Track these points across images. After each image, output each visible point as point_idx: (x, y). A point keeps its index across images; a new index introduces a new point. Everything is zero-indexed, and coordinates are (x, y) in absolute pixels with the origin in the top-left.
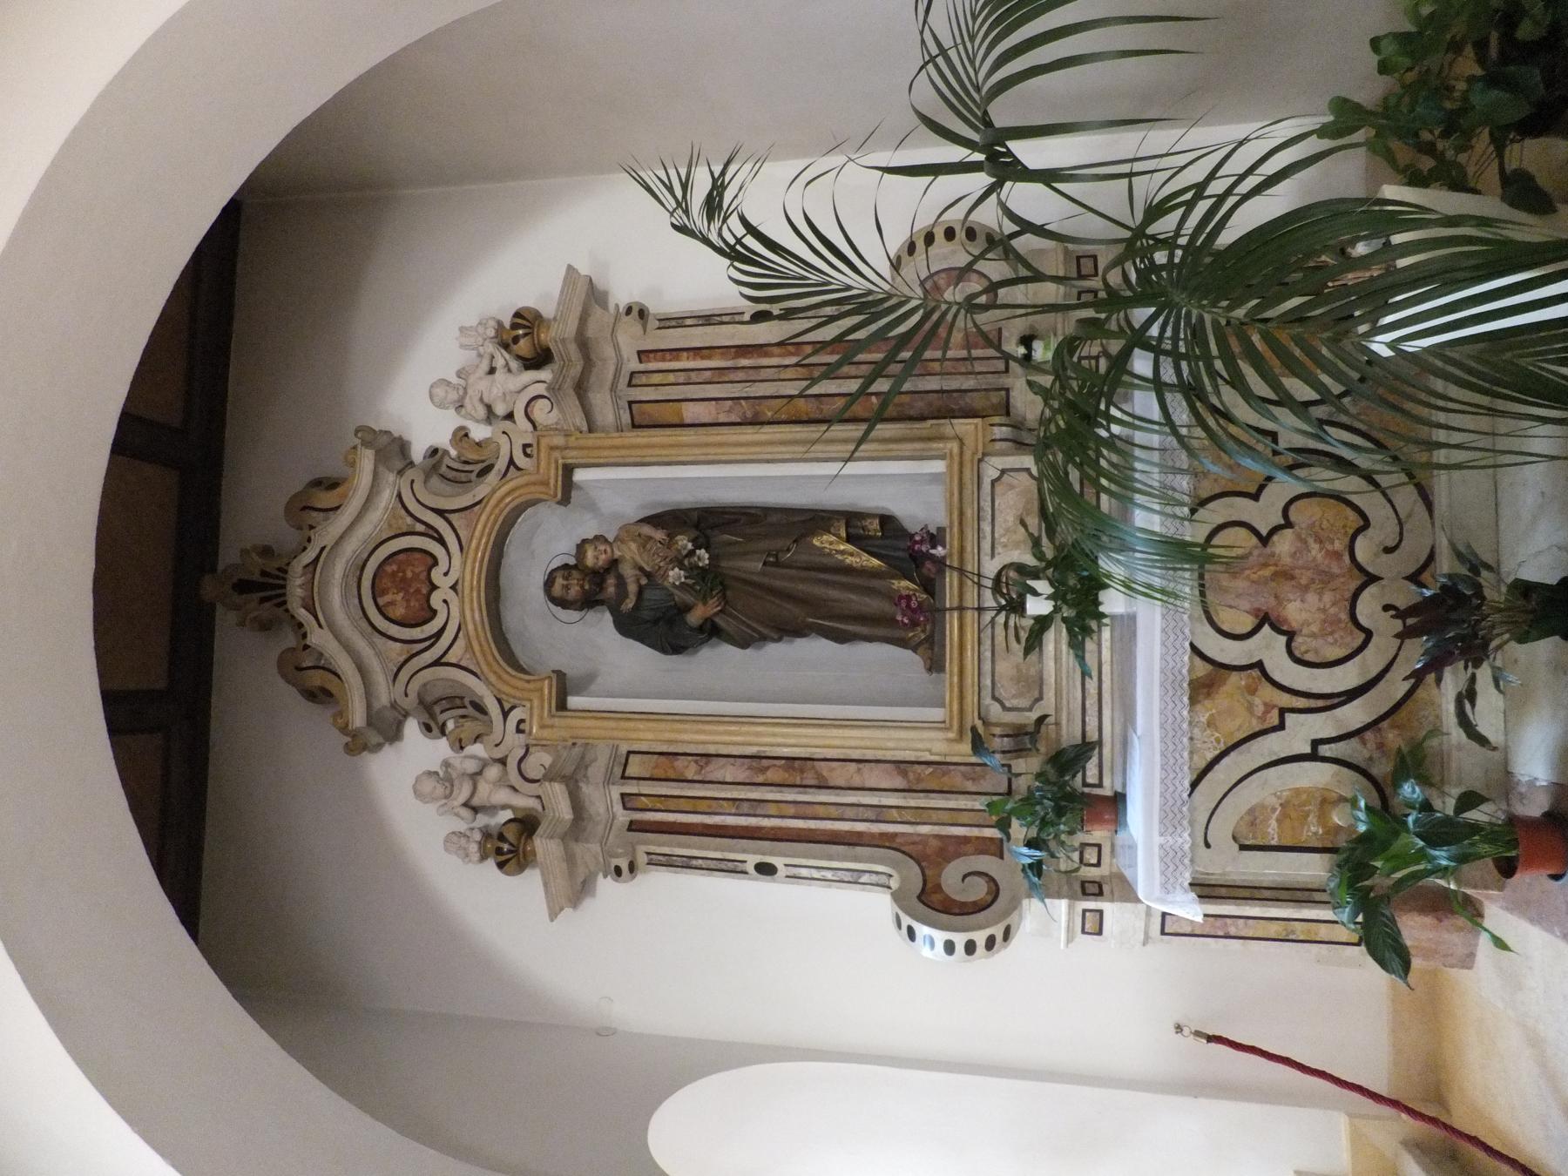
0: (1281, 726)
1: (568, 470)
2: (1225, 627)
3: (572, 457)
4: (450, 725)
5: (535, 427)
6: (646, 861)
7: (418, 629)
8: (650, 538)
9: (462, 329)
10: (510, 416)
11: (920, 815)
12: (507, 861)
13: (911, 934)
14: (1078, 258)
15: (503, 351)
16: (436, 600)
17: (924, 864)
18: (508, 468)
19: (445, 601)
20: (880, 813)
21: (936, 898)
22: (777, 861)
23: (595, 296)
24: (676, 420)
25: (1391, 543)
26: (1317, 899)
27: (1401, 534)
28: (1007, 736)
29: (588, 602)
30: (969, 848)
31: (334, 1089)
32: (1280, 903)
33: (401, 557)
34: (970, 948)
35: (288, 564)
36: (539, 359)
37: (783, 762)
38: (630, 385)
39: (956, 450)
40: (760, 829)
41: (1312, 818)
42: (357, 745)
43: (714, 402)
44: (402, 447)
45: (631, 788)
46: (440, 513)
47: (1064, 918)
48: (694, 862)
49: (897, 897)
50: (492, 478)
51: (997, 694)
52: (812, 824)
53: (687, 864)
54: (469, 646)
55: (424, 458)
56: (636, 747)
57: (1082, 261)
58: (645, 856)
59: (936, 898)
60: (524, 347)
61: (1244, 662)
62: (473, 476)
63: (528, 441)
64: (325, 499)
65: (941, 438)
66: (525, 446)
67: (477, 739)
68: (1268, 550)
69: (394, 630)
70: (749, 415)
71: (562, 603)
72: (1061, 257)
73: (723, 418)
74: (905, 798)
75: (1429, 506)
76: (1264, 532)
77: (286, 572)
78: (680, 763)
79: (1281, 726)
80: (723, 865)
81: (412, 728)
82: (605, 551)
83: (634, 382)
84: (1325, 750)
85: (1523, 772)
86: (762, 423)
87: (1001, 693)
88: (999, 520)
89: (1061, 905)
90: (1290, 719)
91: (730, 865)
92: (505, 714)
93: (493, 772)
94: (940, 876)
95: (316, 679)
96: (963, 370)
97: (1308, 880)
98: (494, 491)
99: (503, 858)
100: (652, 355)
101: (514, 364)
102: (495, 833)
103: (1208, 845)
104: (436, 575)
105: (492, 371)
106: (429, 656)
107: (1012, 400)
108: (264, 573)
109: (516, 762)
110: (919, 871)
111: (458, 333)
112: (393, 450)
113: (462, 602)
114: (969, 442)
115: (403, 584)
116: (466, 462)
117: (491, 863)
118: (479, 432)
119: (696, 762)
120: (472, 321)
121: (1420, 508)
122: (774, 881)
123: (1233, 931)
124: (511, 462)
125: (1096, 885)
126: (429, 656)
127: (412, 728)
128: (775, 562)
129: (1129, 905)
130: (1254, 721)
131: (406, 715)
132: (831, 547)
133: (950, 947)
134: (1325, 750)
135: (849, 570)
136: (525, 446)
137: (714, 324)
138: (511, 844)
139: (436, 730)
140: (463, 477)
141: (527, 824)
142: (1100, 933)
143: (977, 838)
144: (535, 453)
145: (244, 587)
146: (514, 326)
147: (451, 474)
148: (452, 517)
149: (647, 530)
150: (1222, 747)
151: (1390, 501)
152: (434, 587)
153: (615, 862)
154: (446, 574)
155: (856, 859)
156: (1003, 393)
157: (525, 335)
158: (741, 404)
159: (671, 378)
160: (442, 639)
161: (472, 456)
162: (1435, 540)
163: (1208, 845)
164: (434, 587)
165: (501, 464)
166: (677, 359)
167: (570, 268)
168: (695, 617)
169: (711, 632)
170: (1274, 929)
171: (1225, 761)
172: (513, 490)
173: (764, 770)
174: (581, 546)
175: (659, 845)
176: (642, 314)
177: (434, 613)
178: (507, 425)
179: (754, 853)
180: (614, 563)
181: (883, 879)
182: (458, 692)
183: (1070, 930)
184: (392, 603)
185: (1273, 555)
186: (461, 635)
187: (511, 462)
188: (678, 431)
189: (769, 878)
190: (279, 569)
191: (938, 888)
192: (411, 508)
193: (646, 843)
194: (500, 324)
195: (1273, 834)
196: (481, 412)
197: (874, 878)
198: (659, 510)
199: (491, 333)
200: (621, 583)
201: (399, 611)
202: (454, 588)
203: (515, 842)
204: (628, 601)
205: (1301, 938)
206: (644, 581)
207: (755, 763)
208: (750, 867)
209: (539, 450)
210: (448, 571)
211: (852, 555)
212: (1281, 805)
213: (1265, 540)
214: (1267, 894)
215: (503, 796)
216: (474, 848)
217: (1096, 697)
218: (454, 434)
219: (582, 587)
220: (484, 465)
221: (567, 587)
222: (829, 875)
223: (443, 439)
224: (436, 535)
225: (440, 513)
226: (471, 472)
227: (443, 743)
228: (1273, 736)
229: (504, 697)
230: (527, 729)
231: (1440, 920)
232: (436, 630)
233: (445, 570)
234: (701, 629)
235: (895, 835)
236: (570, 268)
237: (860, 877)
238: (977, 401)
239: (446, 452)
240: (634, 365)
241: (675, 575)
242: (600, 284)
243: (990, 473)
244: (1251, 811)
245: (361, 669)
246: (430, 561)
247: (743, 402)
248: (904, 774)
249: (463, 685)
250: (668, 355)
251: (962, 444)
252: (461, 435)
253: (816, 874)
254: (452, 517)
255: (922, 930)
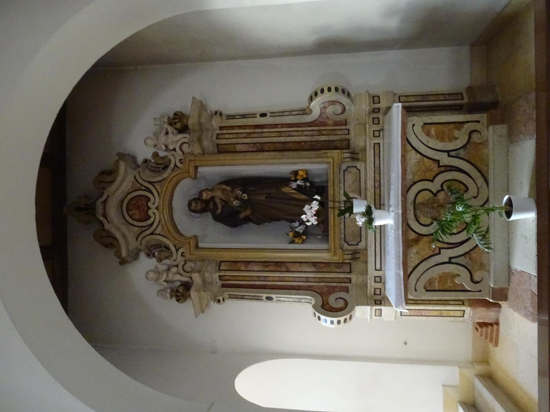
0: (439, 253)
1: (196, 168)
2: (422, 223)
3: (198, 163)
4: (156, 254)
5: (183, 153)
6: (228, 297)
7: (144, 223)
8: (225, 190)
9: (155, 119)
10: (174, 150)
11: (321, 280)
12: (180, 299)
13: (319, 318)
14: (373, 97)
15: (170, 127)
16: (150, 213)
17: (323, 296)
18: (174, 168)
19: (154, 213)
20: (307, 280)
21: (327, 307)
22: (273, 296)
23: (202, 106)
24: (234, 150)
25: (475, 196)
26: (450, 303)
27: (478, 192)
28: (350, 254)
29: (203, 211)
30: (337, 290)
31: (132, 377)
32: (439, 305)
33: (137, 198)
34: (339, 322)
35: (96, 201)
36: (184, 129)
37: (274, 263)
38: (217, 138)
39: (332, 161)
40: (266, 285)
41: (449, 281)
42: (123, 262)
43: (247, 145)
44: (133, 159)
45: (222, 273)
46: (150, 183)
47: (369, 312)
48: (245, 297)
49: (314, 307)
50: (169, 171)
51: (346, 240)
52: (285, 283)
53: (242, 298)
54: (163, 228)
55: (143, 163)
56: (223, 260)
57: (375, 98)
58: (228, 295)
59: (327, 307)
60: (178, 125)
61: (428, 233)
62: (161, 169)
63: (181, 158)
64: (107, 179)
65: (327, 157)
66: (180, 160)
67: (166, 258)
68: (436, 198)
69: (136, 223)
70: (259, 149)
71: (195, 211)
72: (367, 97)
73: (250, 150)
74: (316, 274)
75: (487, 183)
76: (435, 192)
77: (95, 204)
78: (239, 264)
79: (439, 253)
80: (255, 298)
81: (142, 255)
82: (209, 194)
83: (219, 137)
84: (453, 260)
85: (513, 266)
86: (264, 151)
87: (347, 239)
88: (346, 183)
89: (369, 308)
90: (442, 251)
91: (257, 297)
92: (177, 250)
93: (174, 270)
94: (328, 300)
95: (109, 240)
96: (333, 134)
97: (422, 114)
98: (170, 175)
99: (178, 298)
100: (224, 128)
101: (175, 131)
102: (175, 290)
103: (416, 290)
104: (150, 204)
105: (167, 133)
106: (148, 232)
107: (350, 144)
108: (86, 204)
109: (182, 266)
110: (321, 298)
111: (153, 120)
112: (131, 159)
113: (160, 213)
114: (336, 160)
115: (138, 207)
116: (157, 164)
117: (174, 299)
118: (162, 154)
119: (244, 264)
120: (158, 116)
121: (485, 184)
122: (272, 302)
123: (423, 314)
124: (176, 165)
125: (379, 301)
126: (148, 232)
127: (142, 255)
128: (269, 196)
129: (390, 307)
130: (431, 252)
131: (140, 250)
132: (289, 192)
133: (332, 322)
134: (453, 260)
135: (295, 199)
136: (180, 160)
137: (247, 118)
138: (181, 293)
139: (151, 256)
140: (157, 170)
141: (187, 286)
142: (381, 316)
143: (340, 286)
144: (184, 162)
145: (79, 209)
146: (174, 119)
147: (153, 168)
148: (155, 184)
149: (224, 187)
150: (421, 260)
151: (475, 182)
152: (149, 208)
153: (218, 298)
154: (154, 204)
155: (299, 295)
156: (347, 141)
157: (178, 122)
158: (257, 145)
159: (232, 136)
160: (153, 226)
161: (160, 162)
162: (489, 195)
163: (416, 290)
164: (149, 208)
165: (172, 165)
166: (233, 129)
167: (194, 98)
168: (242, 216)
169: (247, 220)
170: (437, 313)
171: (422, 264)
172: (177, 175)
173: (268, 266)
174: (201, 192)
175: (233, 292)
176: (221, 114)
177: (150, 217)
178: (173, 152)
179: (265, 294)
180: (213, 198)
181: (309, 301)
182: (159, 243)
183: (371, 315)
184: (134, 214)
185: (438, 199)
186: (160, 224)
187: (176, 165)
188: (235, 154)
189: (270, 301)
190: (92, 203)
191: (328, 303)
192: (140, 181)
193: (227, 291)
194: (169, 117)
195: (436, 286)
196: (164, 148)
197: (306, 300)
198: (226, 179)
199: (166, 120)
200: (215, 204)
201: (137, 217)
202: (157, 208)
203: (182, 293)
204: (218, 211)
205: (445, 315)
206: (223, 203)
207: (265, 264)
208: (264, 298)
209: (185, 161)
210: (155, 202)
211: (295, 194)
212: (439, 277)
213: (435, 195)
214: (435, 302)
215: (178, 277)
216: (168, 295)
217: (379, 242)
218: (153, 154)
219: (201, 206)
220: (165, 165)
221: (196, 206)
222: (291, 300)
223: (149, 156)
224: (148, 190)
225: (150, 183)
226: (160, 168)
227: (154, 260)
228: (437, 257)
229: (177, 245)
230: (185, 255)
231: (488, 309)
232: (150, 223)
233: (153, 202)
234: (244, 219)
235: (313, 286)
236: (194, 98)
237: (301, 300)
238: (338, 144)
239: (150, 161)
240: (218, 132)
241: (235, 203)
242: (204, 103)
243: (344, 167)
244: (430, 280)
245: (124, 236)
246: (148, 199)
247: (257, 144)
248: (315, 266)
249: (161, 241)
250: (230, 128)
251: (333, 159)
252: (156, 155)
253: (286, 299)
254: (155, 184)
255: (323, 317)
